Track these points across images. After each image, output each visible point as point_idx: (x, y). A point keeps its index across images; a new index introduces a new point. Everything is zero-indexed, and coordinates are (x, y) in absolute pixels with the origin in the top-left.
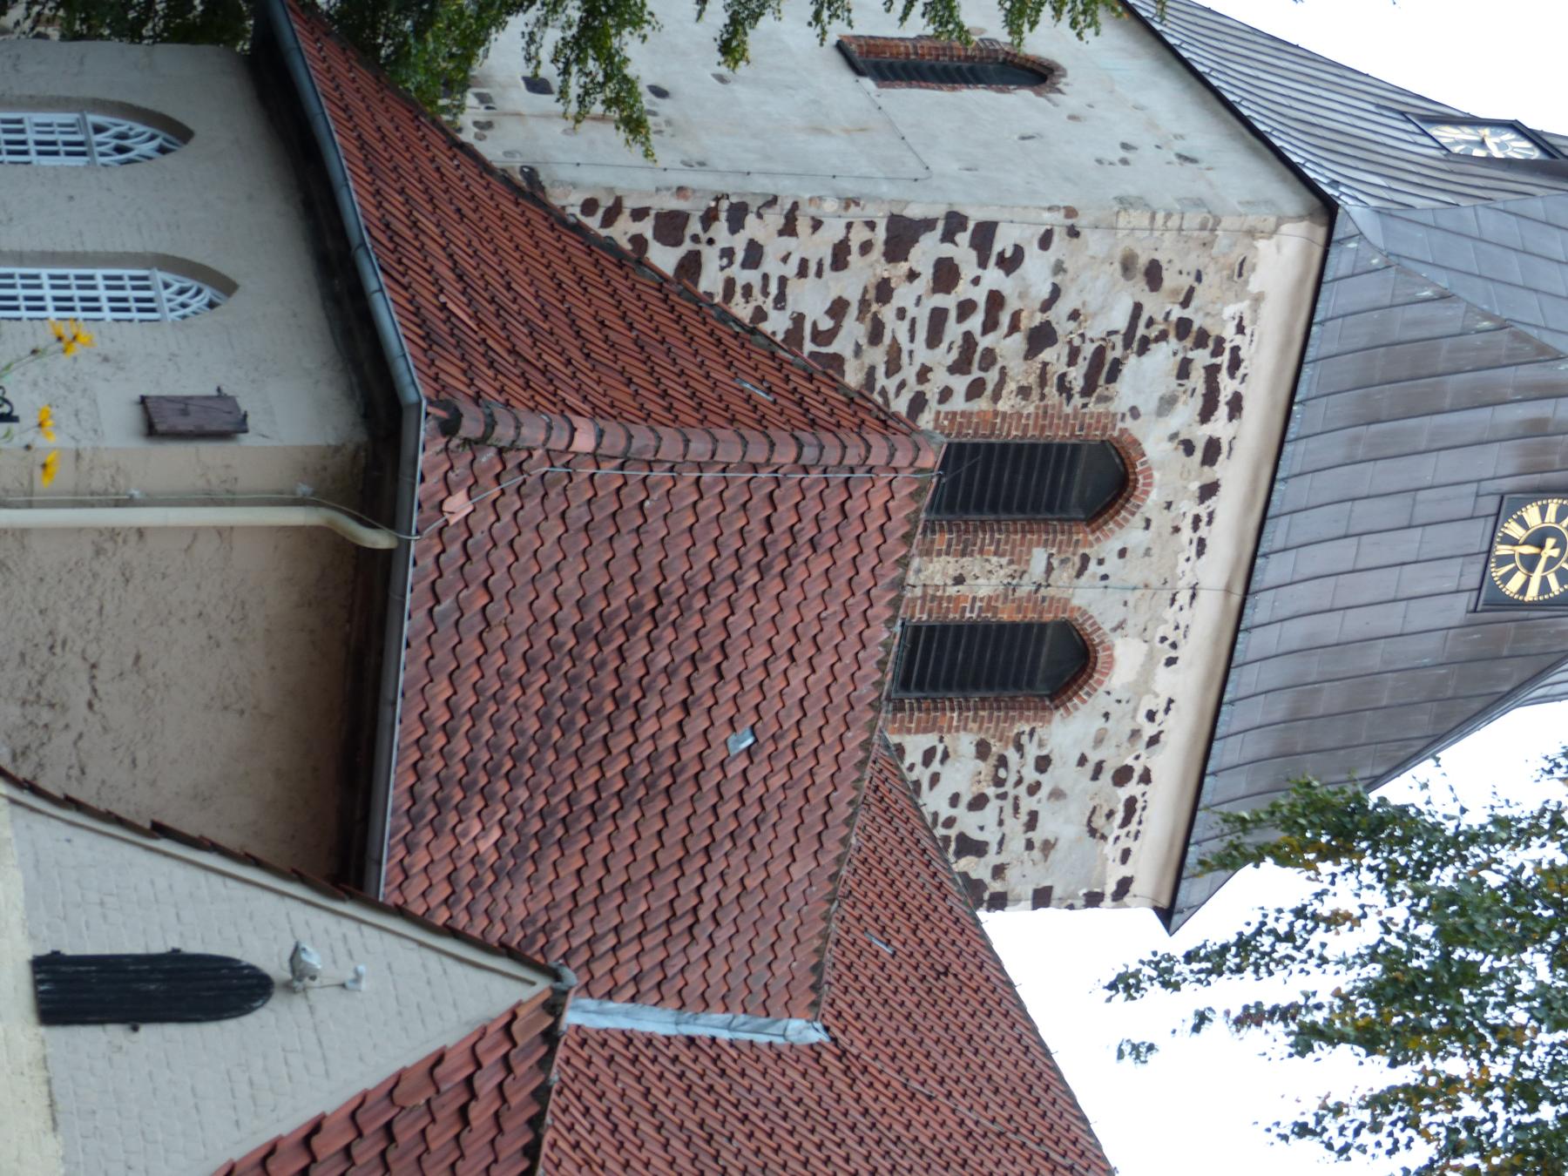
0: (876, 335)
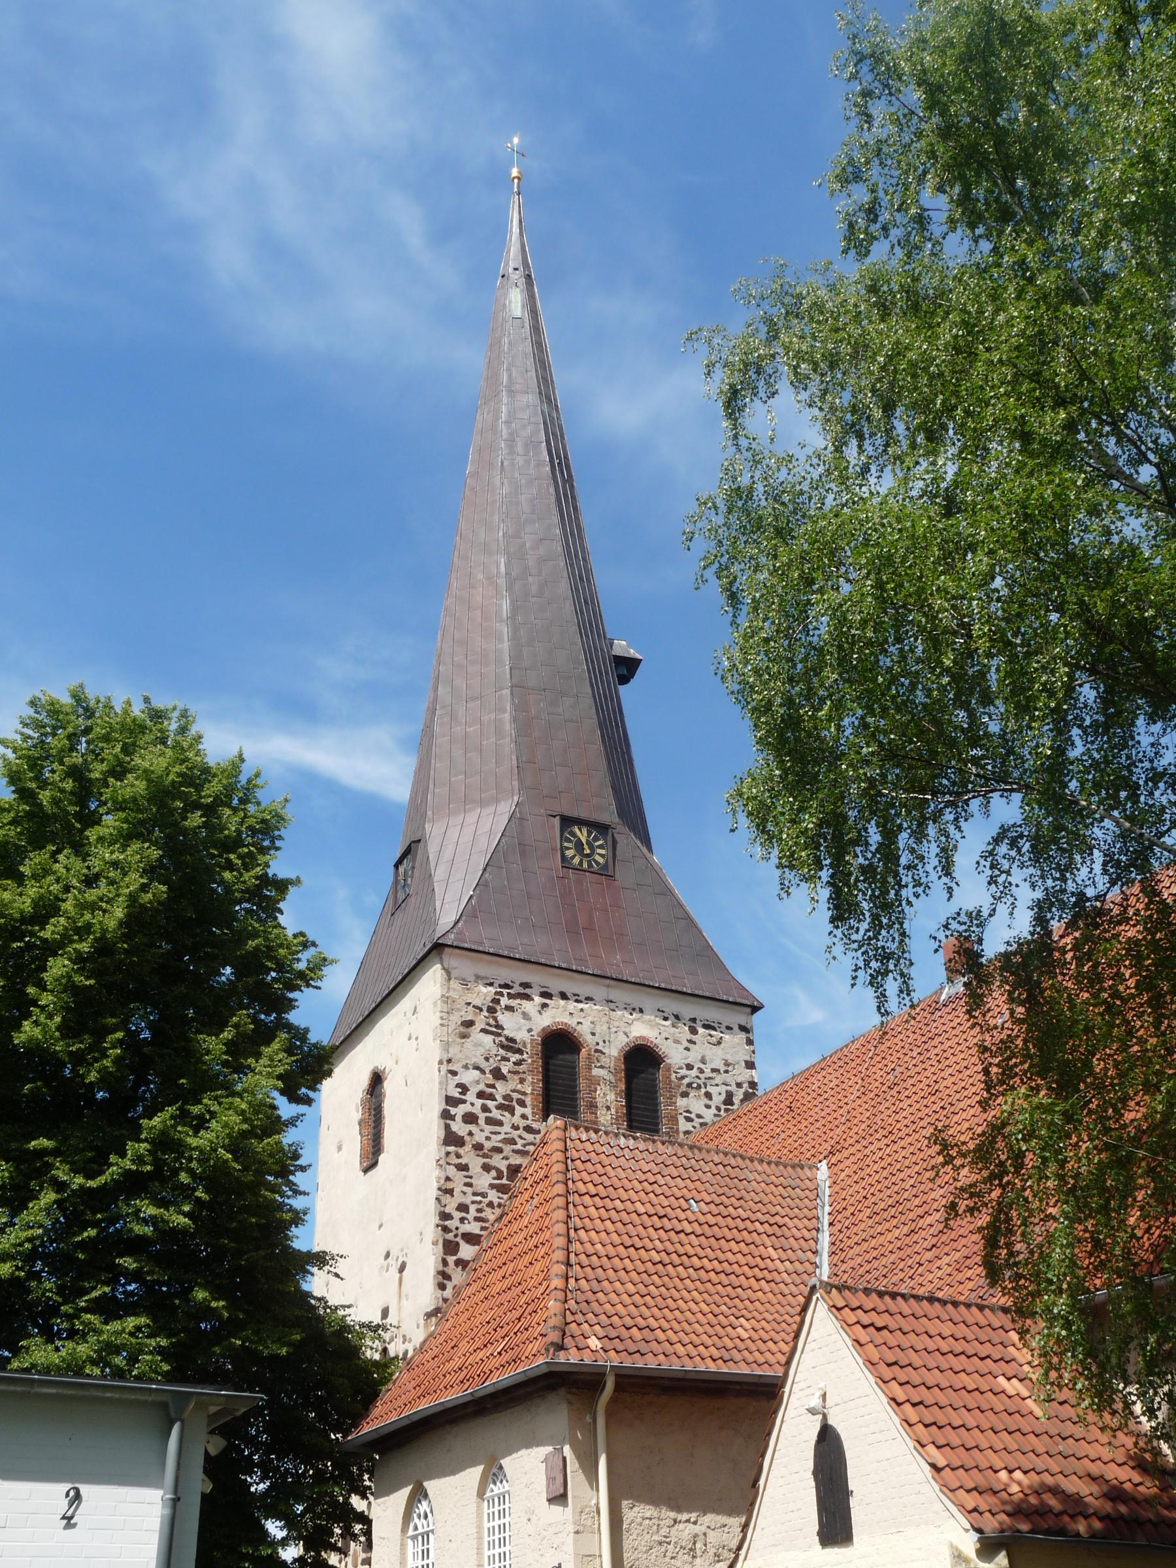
0: (499, 1150)
